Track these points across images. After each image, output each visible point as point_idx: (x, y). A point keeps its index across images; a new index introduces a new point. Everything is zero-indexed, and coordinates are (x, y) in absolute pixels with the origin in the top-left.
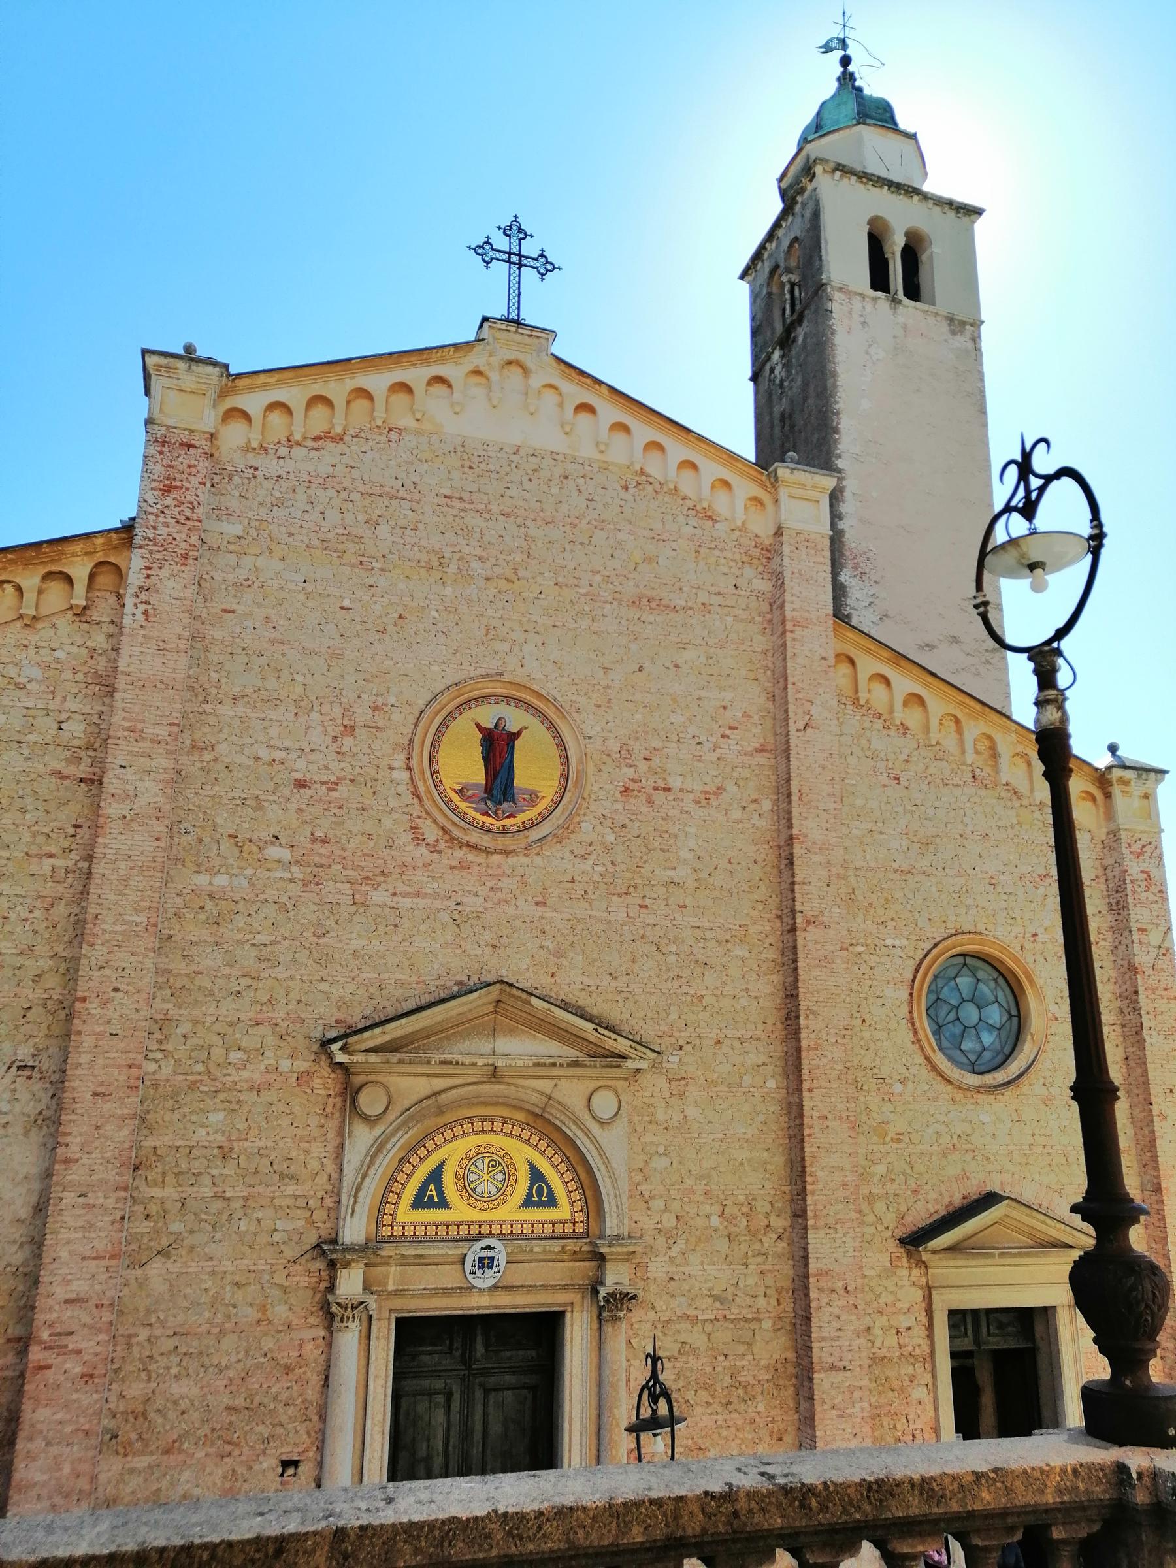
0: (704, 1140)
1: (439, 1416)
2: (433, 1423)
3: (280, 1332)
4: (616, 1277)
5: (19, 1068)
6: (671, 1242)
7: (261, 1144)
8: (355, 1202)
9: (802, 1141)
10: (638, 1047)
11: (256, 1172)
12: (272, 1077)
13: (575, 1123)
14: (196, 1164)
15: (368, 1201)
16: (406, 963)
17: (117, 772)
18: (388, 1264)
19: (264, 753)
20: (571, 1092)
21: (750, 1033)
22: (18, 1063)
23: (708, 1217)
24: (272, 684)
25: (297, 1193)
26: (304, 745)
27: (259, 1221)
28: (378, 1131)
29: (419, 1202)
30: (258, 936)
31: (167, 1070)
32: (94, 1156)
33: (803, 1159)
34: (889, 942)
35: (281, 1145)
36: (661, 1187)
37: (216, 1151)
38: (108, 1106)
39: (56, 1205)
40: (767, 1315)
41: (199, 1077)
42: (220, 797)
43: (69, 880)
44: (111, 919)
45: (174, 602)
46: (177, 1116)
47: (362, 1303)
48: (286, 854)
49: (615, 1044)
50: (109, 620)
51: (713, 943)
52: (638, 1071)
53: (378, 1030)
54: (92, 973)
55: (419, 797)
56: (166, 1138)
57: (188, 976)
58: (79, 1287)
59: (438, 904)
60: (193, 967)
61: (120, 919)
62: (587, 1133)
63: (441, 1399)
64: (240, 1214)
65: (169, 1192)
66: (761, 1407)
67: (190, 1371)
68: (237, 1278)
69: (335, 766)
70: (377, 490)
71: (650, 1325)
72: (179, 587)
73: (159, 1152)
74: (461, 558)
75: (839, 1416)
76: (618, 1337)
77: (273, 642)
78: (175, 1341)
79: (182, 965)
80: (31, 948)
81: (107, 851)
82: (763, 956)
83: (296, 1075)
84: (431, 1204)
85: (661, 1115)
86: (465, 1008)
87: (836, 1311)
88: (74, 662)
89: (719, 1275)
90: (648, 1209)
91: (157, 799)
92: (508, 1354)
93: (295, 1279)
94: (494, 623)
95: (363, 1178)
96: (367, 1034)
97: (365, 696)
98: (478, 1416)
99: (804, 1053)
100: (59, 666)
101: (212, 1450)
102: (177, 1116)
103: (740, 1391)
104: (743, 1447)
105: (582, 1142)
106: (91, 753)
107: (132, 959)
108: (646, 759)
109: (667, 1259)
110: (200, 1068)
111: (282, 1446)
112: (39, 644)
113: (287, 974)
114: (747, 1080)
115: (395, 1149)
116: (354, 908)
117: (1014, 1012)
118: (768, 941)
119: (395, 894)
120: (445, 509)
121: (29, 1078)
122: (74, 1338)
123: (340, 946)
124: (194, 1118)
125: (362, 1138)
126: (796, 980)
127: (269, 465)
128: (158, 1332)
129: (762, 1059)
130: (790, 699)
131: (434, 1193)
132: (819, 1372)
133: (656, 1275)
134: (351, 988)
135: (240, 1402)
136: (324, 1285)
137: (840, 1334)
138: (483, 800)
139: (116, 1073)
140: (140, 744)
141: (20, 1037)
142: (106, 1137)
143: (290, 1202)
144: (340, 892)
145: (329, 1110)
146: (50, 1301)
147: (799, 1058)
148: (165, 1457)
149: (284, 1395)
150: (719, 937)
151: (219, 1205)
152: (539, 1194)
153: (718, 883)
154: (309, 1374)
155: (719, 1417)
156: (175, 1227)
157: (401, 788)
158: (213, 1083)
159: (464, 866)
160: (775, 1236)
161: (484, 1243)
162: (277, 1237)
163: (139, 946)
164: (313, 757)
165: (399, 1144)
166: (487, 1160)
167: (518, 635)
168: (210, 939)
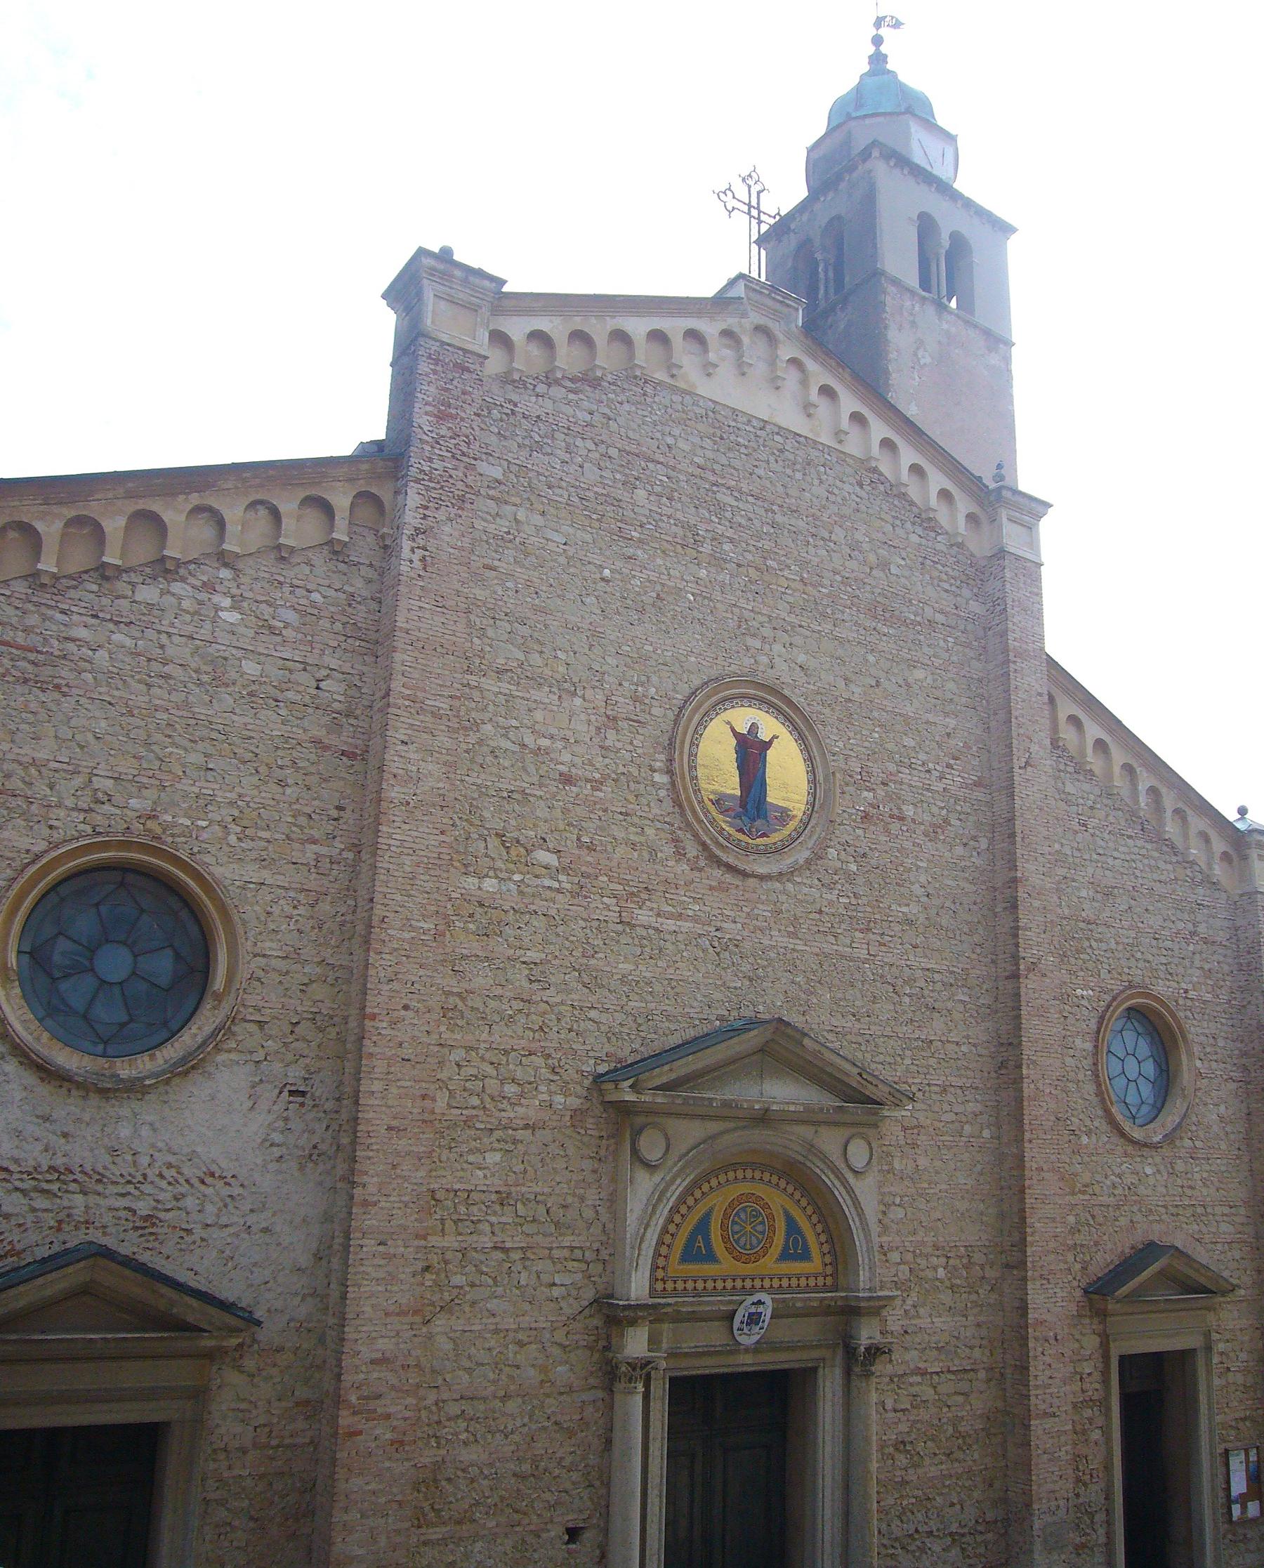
4: (867, 1334)
5: (291, 1093)
7: (538, 1190)
11: (534, 1220)
13: (833, 1172)
14: (475, 1209)
16: (672, 993)
17: (398, 748)
19: (529, 740)
20: (829, 1141)
22: (288, 1088)
23: (935, 1269)
24: (536, 659)
26: (569, 734)
27: (538, 1274)
28: (657, 1178)
29: (687, 1257)
30: (529, 953)
32: (392, 1199)
34: (1079, 992)
36: (898, 1239)
37: (494, 1197)
38: (403, 1142)
39: (357, 1253)
41: (474, 1112)
42: (487, 787)
43: (335, 873)
44: (398, 924)
45: (452, 551)
46: (453, 1156)
47: (649, 1363)
48: (552, 859)
50: (367, 562)
51: (939, 986)
54: (380, 986)
55: (681, 806)
57: (459, 995)
58: (385, 1345)
59: (699, 929)
60: (465, 985)
61: (407, 924)
62: (845, 1183)
66: (976, 1456)
69: (599, 763)
70: (633, 448)
72: (456, 534)
74: (714, 539)
75: (1050, 1460)
77: (536, 609)
78: (465, 1405)
80: (297, 951)
81: (392, 842)
83: (569, 1113)
85: (897, 1165)
87: (1047, 1359)
88: (332, 609)
91: (441, 785)
94: (746, 614)
97: (626, 684)
100: (316, 612)
101: (503, 1519)
102: (453, 1156)
103: (960, 1441)
106: (352, 721)
107: (421, 972)
108: (883, 784)
110: (475, 1101)
112: (296, 582)
113: (558, 999)
114: (967, 1127)
116: (620, 927)
117: (1164, 1067)
118: (985, 987)
119: (658, 915)
120: (698, 481)
121: (302, 1105)
122: (383, 1402)
123: (608, 969)
124: (471, 1158)
125: (643, 1186)
126: (1018, 1027)
127: (527, 403)
128: (445, 1396)
129: (979, 1108)
130: (1014, 734)
135: (526, 1467)
136: (602, 1343)
137: (1050, 1381)
138: (738, 816)
139: (410, 1105)
140: (421, 717)
141: (290, 1057)
142: (405, 1179)
143: (566, 1253)
144: (608, 908)
145: (602, 1152)
146: (356, 1361)
148: (458, 1527)
151: (499, 1255)
153: (944, 922)
156: (458, 1280)
157: (662, 793)
158: (488, 1119)
159: (722, 888)
161: (755, 1298)
162: (556, 1292)
163: (428, 958)
164: (577, 749)
167: (767, 631)
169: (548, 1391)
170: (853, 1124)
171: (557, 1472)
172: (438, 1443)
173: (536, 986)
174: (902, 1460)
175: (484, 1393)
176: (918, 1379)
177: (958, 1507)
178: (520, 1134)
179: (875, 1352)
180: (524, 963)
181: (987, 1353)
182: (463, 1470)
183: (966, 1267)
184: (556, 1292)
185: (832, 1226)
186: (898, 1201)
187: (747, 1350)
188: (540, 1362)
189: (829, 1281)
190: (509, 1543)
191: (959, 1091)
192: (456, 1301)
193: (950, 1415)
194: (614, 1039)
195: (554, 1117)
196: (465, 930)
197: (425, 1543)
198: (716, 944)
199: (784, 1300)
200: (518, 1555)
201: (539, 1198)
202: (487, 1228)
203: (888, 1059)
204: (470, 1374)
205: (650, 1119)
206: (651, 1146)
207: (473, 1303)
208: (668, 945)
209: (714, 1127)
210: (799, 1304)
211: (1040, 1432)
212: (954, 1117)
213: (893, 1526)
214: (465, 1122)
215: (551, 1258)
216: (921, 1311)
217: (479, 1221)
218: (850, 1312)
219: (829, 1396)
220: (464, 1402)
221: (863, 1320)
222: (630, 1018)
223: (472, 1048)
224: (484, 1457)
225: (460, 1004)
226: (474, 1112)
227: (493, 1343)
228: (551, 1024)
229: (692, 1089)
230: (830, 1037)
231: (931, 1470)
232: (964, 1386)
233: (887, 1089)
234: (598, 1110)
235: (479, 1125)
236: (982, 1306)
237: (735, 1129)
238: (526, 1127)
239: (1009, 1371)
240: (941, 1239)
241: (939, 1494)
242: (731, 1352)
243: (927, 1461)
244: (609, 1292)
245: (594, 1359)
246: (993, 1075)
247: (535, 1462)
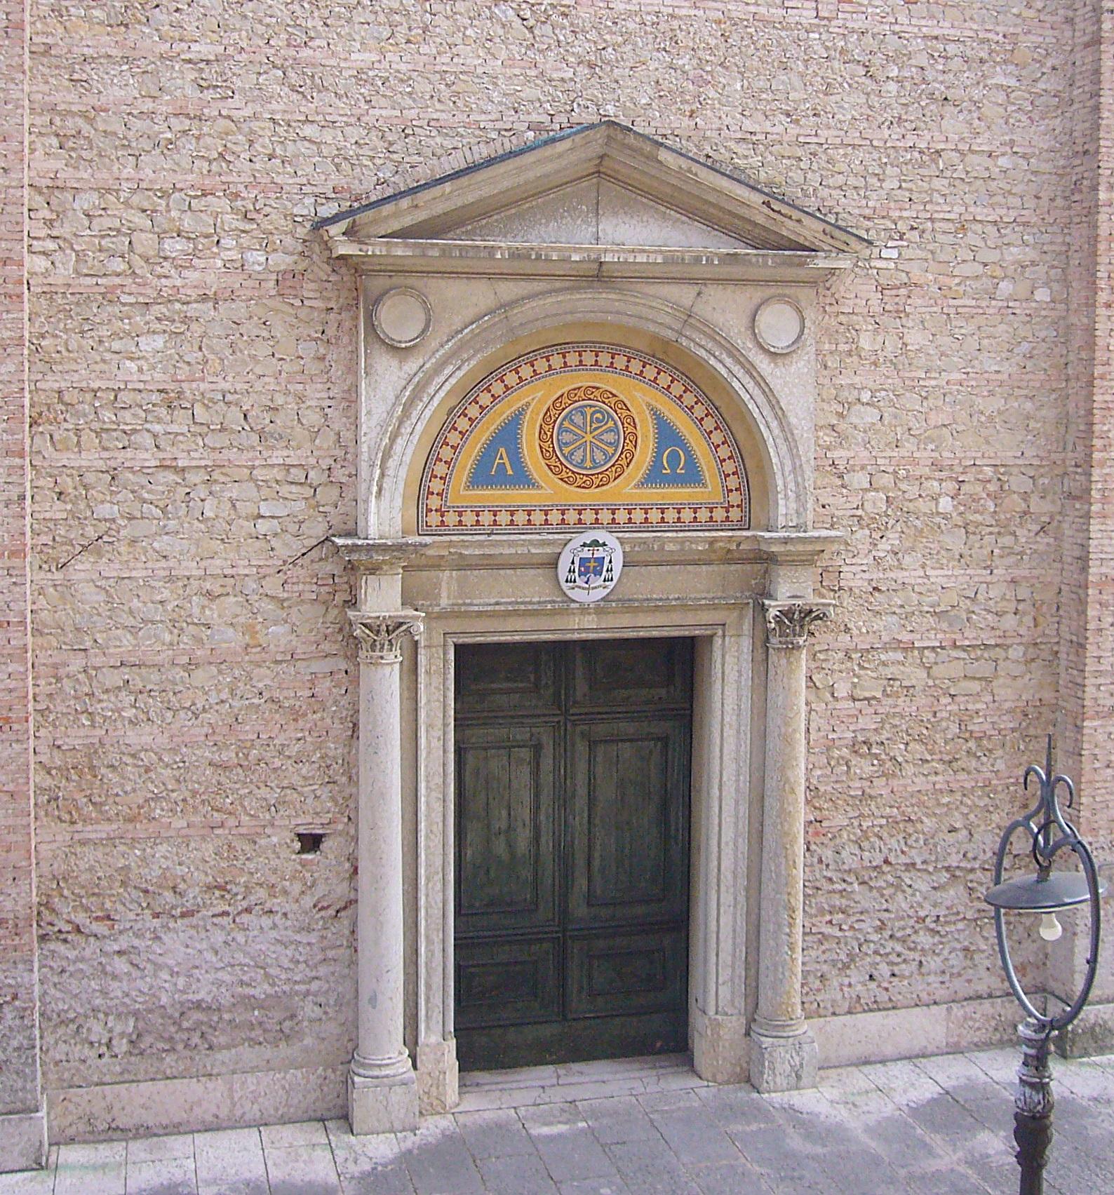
0: (933, 383)
1: (523, 776)
2: (515, 783)
3: (277, 662)
4: (789, 590)
6: (876, 535)
7: (226, 386)
8: (383, 475)
9: (1091, 384)
10: (837, 233)
12: (235, 281)
13: (730, 354)
14: (127, 416)
15: (403, 473)
18: (437, 567)
20: (725, 309)
21: (1013, 214)
23: (935, 499)
25: (288, 461)
28: (412, 366)
29: (483, 476)
31: (65, 271)
33: (1090, 412)
35: (258, 386)
37: (155, 398)
40: (1018, 640)
41: (117, 281)
47: (401, 624)
49: (798, 228)
51: (956, 63)
52: (832, 272)
53: (405, 203)
56: (76, 377)
57: (83, 115)
60: (92, 100)
62: (751, 369)
63: (525, 754)
64: (202, 492)
65: (91, 458)
66: (1000, 765)
67: (152, 714)
68: (208, 586)
71: (841, 655)
73: (67, 398)
76: (797, 672)
78: (126, 673)
79: (72, 97)
82: (1041, 85)
84: (501, 479)
85: (865, 343)
86: (549, 168)
89: (947, 579)
90: (843, 486)
92: (624, 693)
93: (296, 588)
95: (393, 440)
96: (387, 209)
98: (581, 778)
99: (1102, 247)
101: (197, 819)
103: (972, 744)
104: (972, 816)
105: (742, 385)
109: (871, 560)
110: (119, 265)
111: (297, 816)
113: (247, 112)
114: (1005, 287)
115: (442, 394)
123: (333, 62)
124: (116, 345)
125: (384, 383)
128: (98, 661)
129: (1032, 254)
131: (506, 460)
132: (1093, 719)
133: (852, 584)
134: (355, 133)
135: (229, 756)
136: (339, 598)
145: (331, 331)
147: (1095, 254)
148: (130, 827)
149: (294, 749)
150: (969, 53)
151: (172, 477)
152: (673, 465)
154: (329, 721)
155: (939, 778)
156: (105, 510)
160: (1036, 528)
161: (588, 537)
162: (263, 526)
165: (447, 387)
166: (589, 411)
168: (113, 52)
169: (258, 658)
170: (767, 282)
171: (277, 763)
172: (93, 721)
173: (209, 95)
174: (863, 767)
175: (158, 659)
176: (899, 656)
177: (965, 832)
178: (194, 309)
179: (801, 619)
180: (190, 61)
181: (1028, 620)
182: (133, 756)
183: (993, 497)
184: (263, 526)
185: (741, 436)
186: (866, 396)
187: (584, 610)
188: (242, 619)
189: (735, 514)
190: (209, 849)
191: (991, 230)
192: (106, 538)
193: (954, 707)
194: (345, 166)
195: (249, 283)
196: (87, 18)
197: (83, 843)
198: (528, 14)
199: (644, 542)
200: (224, 864)
201: (229, 397)
202: (149, 441)
203: (852, 181)
204: (135, 635)
205: (396, 280)
206: (398, 318)
207: (133, 542)
208: (439, 20)
209: (509, 290)
210: (670, 547)
211: (1101, 737)
212: (980, 269)
213: (844, 854)
214: (104, 295)
215: (251, 478)
216: (907, 560)
217: (135, 431)
218: (765, 561)
219: (732, 676)
220: (127, 670)
221: (782, 571)
222: (374, 133)
223: (108, 190)
224: (163, 740)
225: (86, 129)
226: (117, 281)
227: (166, 594)
228: (237, 149)
229: (470, 235)
230: (741, 149)
231: (913, 780)
232: (985, 669)
233: (820, 226)
234: (323, 270)
235: (124, 299)
236: (1022, 553)
237: (550, 292)
238: (204, 298)
239: (1063, 649)
240: (945, 454)
241: (927, 815)
242: (553, 613)
243: (909, 770)
244: (351, 525)
245: (330, 617)
246: (1060, 202)
247: (243, 747)
